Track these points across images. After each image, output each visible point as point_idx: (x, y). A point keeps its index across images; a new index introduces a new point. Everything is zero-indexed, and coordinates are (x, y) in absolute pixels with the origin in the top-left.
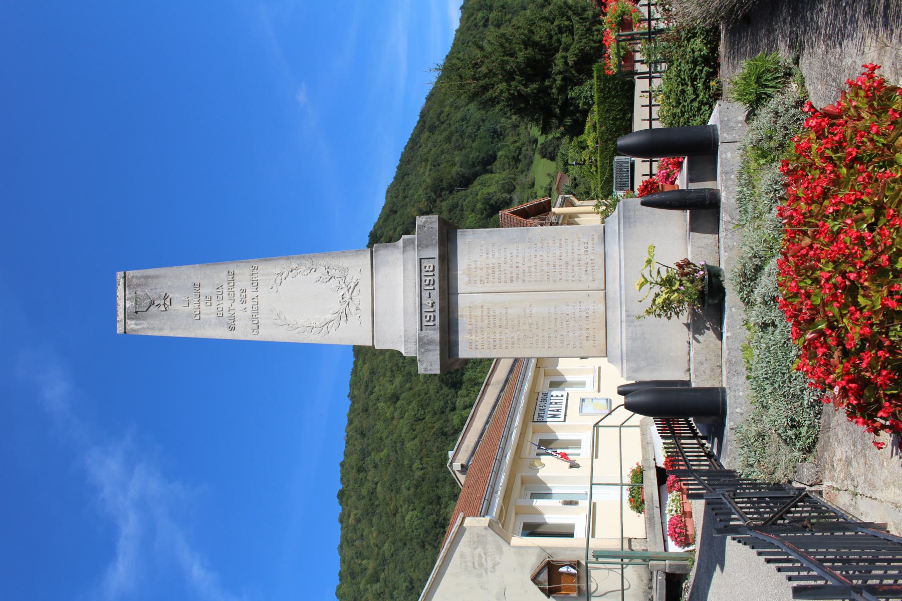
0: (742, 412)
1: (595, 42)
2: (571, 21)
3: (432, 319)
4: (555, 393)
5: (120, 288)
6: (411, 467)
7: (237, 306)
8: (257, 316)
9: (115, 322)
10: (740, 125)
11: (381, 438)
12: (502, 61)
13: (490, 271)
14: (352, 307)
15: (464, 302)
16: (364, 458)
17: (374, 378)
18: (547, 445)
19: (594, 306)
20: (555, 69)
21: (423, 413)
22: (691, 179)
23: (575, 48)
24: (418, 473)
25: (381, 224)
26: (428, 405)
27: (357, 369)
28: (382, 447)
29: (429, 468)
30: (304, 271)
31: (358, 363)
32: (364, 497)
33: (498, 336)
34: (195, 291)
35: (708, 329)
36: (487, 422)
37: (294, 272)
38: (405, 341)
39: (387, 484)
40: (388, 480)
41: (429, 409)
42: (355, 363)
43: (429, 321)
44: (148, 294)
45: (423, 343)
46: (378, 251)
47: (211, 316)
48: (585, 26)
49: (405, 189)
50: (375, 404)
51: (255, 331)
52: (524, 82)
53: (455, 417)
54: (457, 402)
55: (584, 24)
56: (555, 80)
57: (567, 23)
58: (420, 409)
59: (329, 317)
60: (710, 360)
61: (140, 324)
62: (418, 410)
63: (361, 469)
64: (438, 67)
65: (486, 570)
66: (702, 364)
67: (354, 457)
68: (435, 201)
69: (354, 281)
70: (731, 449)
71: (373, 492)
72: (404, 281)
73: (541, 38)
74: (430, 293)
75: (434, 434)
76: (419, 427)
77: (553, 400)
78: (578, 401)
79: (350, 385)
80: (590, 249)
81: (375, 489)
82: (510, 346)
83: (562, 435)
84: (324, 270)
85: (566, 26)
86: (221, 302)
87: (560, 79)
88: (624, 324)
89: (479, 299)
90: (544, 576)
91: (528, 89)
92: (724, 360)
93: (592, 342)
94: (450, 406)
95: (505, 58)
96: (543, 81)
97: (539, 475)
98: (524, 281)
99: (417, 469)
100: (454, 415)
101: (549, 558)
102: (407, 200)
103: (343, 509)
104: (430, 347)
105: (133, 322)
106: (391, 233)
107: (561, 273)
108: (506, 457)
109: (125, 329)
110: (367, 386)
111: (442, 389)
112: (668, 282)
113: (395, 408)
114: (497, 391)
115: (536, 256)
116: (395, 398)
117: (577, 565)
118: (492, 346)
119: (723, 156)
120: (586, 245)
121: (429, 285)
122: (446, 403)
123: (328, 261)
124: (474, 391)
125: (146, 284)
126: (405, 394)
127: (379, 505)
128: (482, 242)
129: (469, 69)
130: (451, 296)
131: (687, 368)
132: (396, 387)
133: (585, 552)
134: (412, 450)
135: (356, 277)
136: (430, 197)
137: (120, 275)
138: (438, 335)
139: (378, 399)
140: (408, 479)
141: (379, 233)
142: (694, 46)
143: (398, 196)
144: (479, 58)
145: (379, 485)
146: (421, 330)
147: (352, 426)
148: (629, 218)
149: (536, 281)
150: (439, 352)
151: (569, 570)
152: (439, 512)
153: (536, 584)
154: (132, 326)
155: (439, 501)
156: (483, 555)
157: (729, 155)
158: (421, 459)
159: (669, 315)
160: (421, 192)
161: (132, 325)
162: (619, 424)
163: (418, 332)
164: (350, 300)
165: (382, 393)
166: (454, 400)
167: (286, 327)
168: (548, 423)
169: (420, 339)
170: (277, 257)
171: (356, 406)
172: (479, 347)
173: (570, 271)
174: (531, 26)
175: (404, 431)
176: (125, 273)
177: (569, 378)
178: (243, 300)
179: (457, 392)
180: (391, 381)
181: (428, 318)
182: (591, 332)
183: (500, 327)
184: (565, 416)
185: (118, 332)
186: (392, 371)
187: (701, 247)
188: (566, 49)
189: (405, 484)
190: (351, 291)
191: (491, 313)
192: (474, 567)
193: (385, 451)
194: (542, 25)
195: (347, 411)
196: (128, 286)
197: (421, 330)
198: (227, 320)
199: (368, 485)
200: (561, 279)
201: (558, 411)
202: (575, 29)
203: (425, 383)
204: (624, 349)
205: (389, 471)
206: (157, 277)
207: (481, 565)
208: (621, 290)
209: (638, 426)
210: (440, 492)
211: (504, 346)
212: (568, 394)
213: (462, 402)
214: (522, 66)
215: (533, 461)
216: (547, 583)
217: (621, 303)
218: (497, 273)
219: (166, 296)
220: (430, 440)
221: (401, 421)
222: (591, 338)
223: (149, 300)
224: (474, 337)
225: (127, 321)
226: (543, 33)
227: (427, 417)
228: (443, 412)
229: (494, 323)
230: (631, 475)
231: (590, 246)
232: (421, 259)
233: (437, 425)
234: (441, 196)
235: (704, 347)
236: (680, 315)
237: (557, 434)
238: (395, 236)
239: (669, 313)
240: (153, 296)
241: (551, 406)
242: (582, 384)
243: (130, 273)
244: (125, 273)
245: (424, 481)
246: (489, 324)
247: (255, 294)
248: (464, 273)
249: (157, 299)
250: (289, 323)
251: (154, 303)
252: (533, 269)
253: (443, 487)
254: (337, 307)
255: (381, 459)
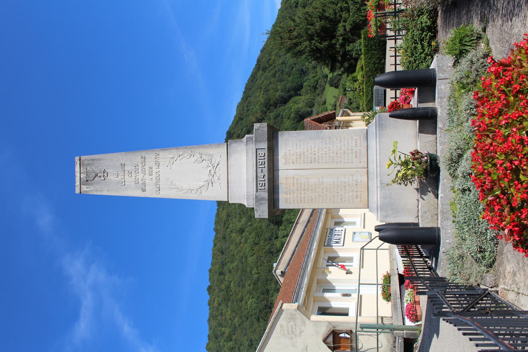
0: (450, 242)
1: (362, 17)
2: (348, 4)
3: (263, 185)
4: (337, 229)
5: (77, 166)
6: (251, 272)
7: (147, 177)
8: (158, 183)
9: (74, 187)
10: (449, 69)
11: (233, 255)
12: (307, 28)
13: (298, 157)
14: (216, 178)
15: (283, 175)
16: (223, 267)
17: (229, 219)
18: (333, 260)
19: (361, 178)
20: (338, 33)
21: (258, 240)
22: (420, 101)
23: (350, 20)
24: (256, 276)
25: (233, 126)
26: (262, 235)
27: (219, 214)
28: (234, 260)
29: (262, 273)
30: (187, 156)
31: (220, 210)
32: (223, 290)
33: (303, 195)
34: (122, 168)
35: (430, 192)
36: (297, 246)
37: (181, 157)
38: (247, 198)
39: (237, 282)
40: (237, 280)
41: (262, 237)
42: (218, 210)
43: (262, 186)
44: (94, 170)
45: (258, 199)
46: (231, 144)
47: (131, 183)
48: (356, 7)
49: (248, 105)
50: (230, 235)
51: (158, 192)
52: (320, 41)
53: (278, 242)
54: (279, 234)
55: (356, 6)
56: (338, 40)
57: (345, 5)
58: (257, 237)
59: (202, 184)
60: (431, 211)
61: (89, 188)
62: (256, 238)
63: (221, 274)
64: (268, 32)
65: (296, 335)
66: (426, 213)
67: (217, 266)
68: (266, 113)
69: (217, 162)
70: (443, 265)
71: (228, 287)
72: (247, 162)
73: (330, 14)
74: (262, 170)
75: (265, 252)
76: (256, 248)
77: (336, 233)
78: (352, 234)
79: (215, 223)
80: (358, 143)
81: (230, 285)
82: (310, 201)
83: (341, 254)
84: (199, 156)
85: (345, 7)
86: (137, 175)
87: (341, 39)
88: (379, 189)
89: (291, 173)
90: (330, 339)
91: (322, 45)
92: (439, 210)
93: (359, 200)
94: (275, 236)
95: (308, 27)
96: (331, 40)
97: (327, 278)
98: (318, 162)
99: (255, 273)
100: (277, 241)
101: (333, 328)
102: (249, 112)
103: (211, 297)
104: (262, 202)
105: (85, 187)
106: (239, 132)
107: (341, 158)
108: (308, 267)
109: (80, 191)
110: (225, 224)
111: (270, 225)
112: (405, 163)
113: (242, 237)
114: (303, 228)
115: (326, 148)
116: (242, 231)
117: (350, 332)
118: (299, 202)
119: (439, 87)
120: (356, 141)
121: (262, 164)
122: (272, 234)
123: (201, 150)
124: (289, 227)
125: (93, 164)
126: (248, 228)
127: (232, 295)
128: (294, 139)
129: (286, 33)
130: (275, 172)
131: (417, 215)
132: (242, 224)
133: (355, 325)
134: (252, 262)
135: (218, 160)
136: (263, 110)
137: (77, 158)
138: (267, 195)
139: (231, 232)
140: (249, 279)
141: (232, 132)
142: (422, 20)
143: (244, 110)
144: (292, 27)
145: (232, 283)
146: (257, 192)
147: (216, 247)
148: (382, 124)
149: (326, 162)
150: (267, 205)
151: (345, 335)
152: (268, 299)
153: (326, 344)
154: (85, 189)
155: (268, 293)
156: (294, 326)
157: (443, 87)
158: (257, 268)
159: (406, 184)
160: (257, 107)
161: (84, 188)
162: (376, 248)
163: (255, 193)
164: (214, 174)
165: (234, 228)
166: (277, 232)
167: (176, 190)
168: (333, 247)
169: (256, 197)
170: (171, 148)
171: (218, 235)
172: (292, 202)
173: (346, 156)
174: (324, 7)
175: (247, 250)
176: (80, 157)
177: (346, 220)
178: (150, 173)
179: (279, 227)
180: (239, 221)
181: (261, 184)
182: (359, 193)
183: (304, 190)
184: (344, 242)
185: (76, 193)
186: (240, 215)
187: (425, 142)
188: (345, 21)
189: (247, 282)
190: (215, 168)
191: (299, 182)
192: (288, 333)
193: (236, 263)
194: (331, 6)
195: (213, 238)
196: (83, 165)
197: (257, 192)
198: (141, 185)
199: (226, 283)
200: (341, 161)
201: (339, 239)
202: (350, 9)
203: (260, 222)
204: (379, 203)
205: (238, 274)
206: (99, 160)
207: (293, 332)
208: (377, 168)
209: (388, 249)
210: (269, 287)
211: (306, 202)
212: (345, 229)
213: (282, 234)
214: (318, 32)
215: (324, 270)
216: (332, 343)
217: (377, 176)
218: (302, 158)
219: (105, 171)
220: (263, 256)
221: (246, 244)
222: (359, 197)
223: (95, 174)
224: (288, 196)
225: (82, 186)
226: (331, 11)
227: (261, 242)
228: (270, 240)
229: (301, 188)
230: (383, 278)
231: (358, 141)
232: (257, 149)
233: (267, 247)
234: (269, 109)
235: (427, 203)
236: (413, 183)
237: (339, 253)
238: (242, 134)
239: (406, 182)
240: (97, 171)
241: (335, 236)
242: (354, 223)
243: (83, 158)
244: (80, 157)
245: (259, 280)
246: (297, 188)
247: (158, 170)
248: (282, 158)
249: (99, 173)
250: (178, 187)
251: (97, 175)
252: (324, 155)
253: (270, 284)
254: (207, 177)
255: (233, 268)
